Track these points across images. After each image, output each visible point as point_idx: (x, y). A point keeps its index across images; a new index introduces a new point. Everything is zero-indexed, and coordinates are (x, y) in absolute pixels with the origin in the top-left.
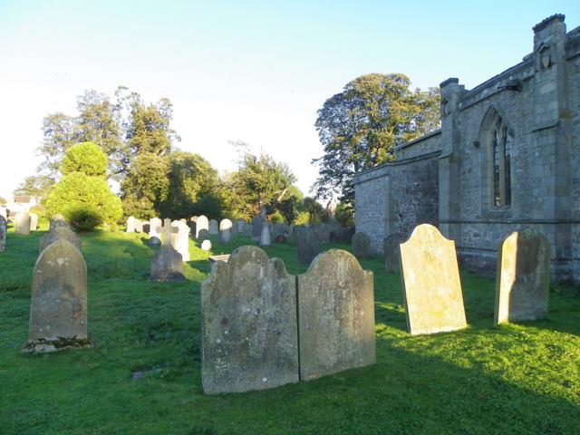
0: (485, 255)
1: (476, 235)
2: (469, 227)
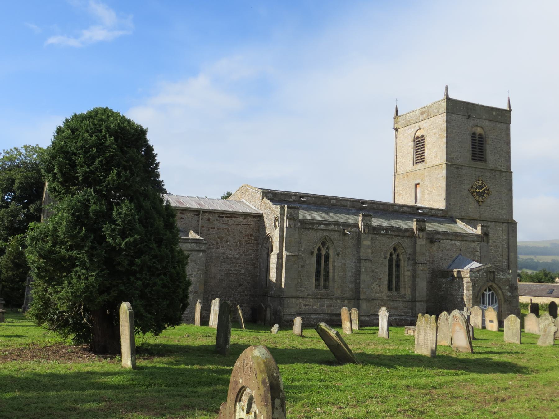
0: (312, 316)
1: (305, 305)
2: (300, 300)
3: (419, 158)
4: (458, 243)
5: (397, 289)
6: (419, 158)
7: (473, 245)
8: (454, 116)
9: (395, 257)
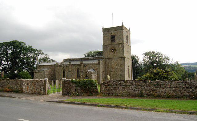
3: (127, 37)
4: (92, 66)
5: (79, 77)
6: (127, 37)
7: (96, 66)
8: (105, 33)
9: (64, 70)
